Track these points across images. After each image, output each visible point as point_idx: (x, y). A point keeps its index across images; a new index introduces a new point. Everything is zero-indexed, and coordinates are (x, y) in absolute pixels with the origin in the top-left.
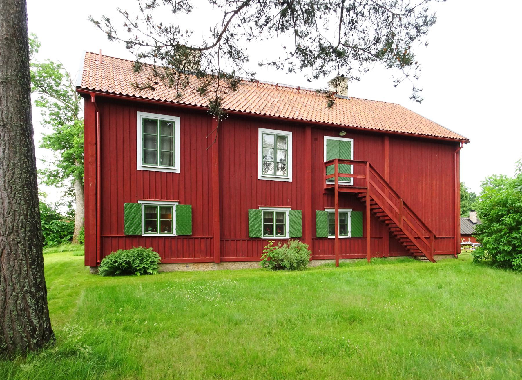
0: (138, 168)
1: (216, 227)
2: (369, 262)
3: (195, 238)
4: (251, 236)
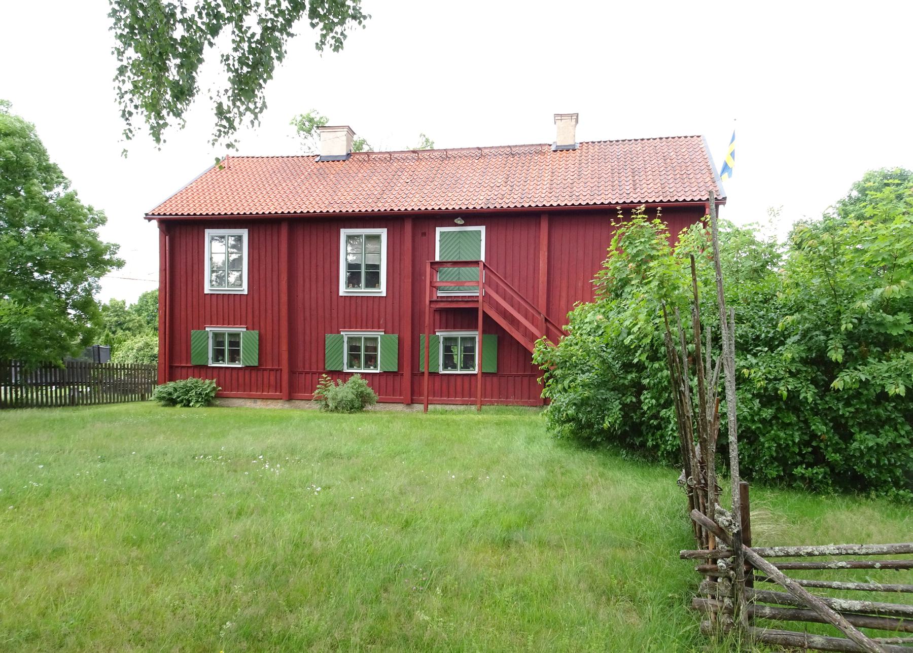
0: (206, 292)
1: (285, 356)
2: (479, 410)
3: (264, 370)
4: (328, 369)
